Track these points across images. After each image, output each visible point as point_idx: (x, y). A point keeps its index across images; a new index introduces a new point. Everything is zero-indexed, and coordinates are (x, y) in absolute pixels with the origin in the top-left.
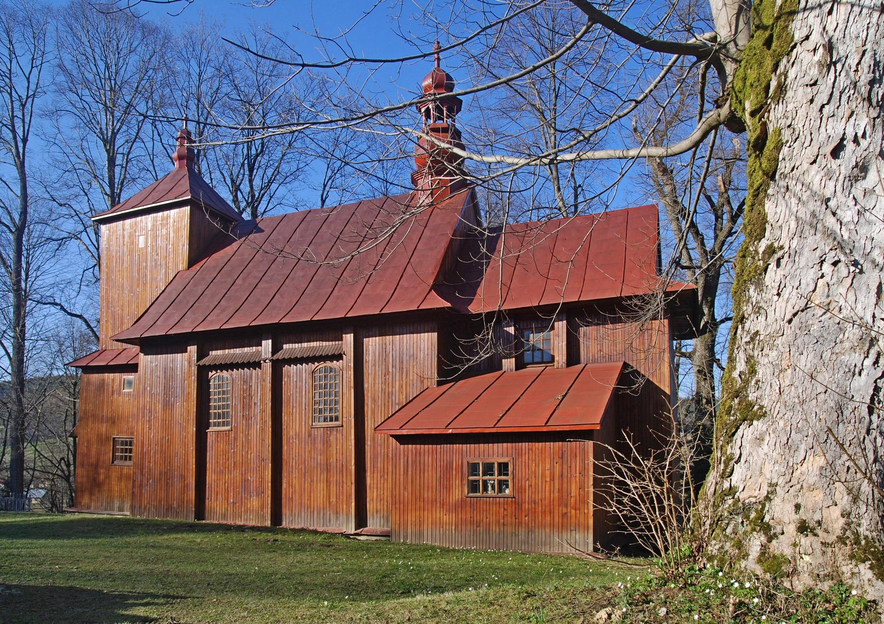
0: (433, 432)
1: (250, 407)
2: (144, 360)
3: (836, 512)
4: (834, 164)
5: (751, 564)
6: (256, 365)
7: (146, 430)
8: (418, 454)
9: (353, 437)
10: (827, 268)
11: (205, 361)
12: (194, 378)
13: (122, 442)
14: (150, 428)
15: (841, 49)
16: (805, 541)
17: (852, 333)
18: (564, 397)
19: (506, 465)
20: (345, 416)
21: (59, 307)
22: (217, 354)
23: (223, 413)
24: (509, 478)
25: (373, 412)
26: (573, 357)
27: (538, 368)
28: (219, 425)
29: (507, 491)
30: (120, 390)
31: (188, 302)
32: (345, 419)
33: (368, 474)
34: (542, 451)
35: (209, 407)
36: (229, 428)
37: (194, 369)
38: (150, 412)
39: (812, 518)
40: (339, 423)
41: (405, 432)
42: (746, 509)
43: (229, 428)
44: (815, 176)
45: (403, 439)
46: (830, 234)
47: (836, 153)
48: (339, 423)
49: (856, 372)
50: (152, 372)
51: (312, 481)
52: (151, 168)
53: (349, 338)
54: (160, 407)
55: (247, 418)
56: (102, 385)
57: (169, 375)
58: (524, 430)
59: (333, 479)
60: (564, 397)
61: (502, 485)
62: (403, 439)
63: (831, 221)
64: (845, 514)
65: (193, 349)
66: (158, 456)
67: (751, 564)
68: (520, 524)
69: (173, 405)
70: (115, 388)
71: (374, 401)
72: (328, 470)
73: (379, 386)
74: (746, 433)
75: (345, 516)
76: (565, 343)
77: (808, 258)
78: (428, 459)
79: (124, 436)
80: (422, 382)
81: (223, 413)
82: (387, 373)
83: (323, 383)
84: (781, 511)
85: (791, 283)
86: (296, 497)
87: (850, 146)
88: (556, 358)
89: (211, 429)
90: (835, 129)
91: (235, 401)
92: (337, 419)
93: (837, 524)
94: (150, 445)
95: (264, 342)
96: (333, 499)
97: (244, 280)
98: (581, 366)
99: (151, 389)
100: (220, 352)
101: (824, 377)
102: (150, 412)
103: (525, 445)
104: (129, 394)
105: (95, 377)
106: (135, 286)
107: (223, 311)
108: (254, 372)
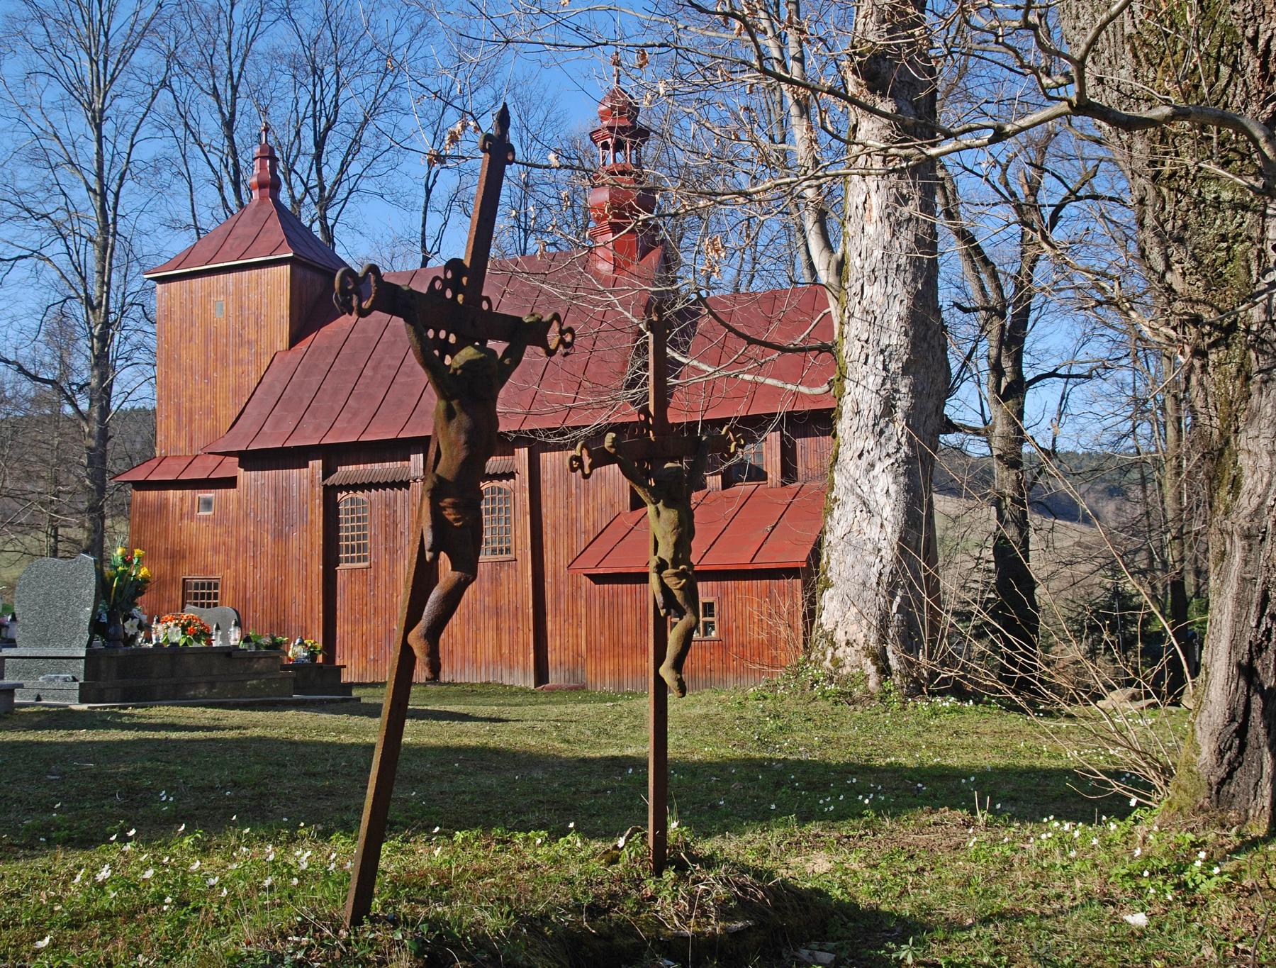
0: (633, 571)
1: (395, 537)
2: (242, 474)
3: (862, 635)
4: (859, 462)
5: (827, 664)
6: (405, 484)
7: (250, 569)
8: (615, 594)
9: (530, 573)
10: (858, 513)
11: (334, 479)
12: (319, 502)
13: (197, 584)
14: (255, 567)
15: (861, 406)
16: (848, 650)
17: (870, 546)
18: (774, 527)
19: (711, 605)
20: (519, 547)
21: (15, 367)
22: (347, 471)
23: (359, 545)
24: (715, 619)
25: (554, 543)
26: (789, 471)
27: (751, 486)
28: (353, 560)
29: (713, 634)
30: (193, 513)
31: (301, 401)
32: (518, 552)
33: (549, 618)
34: (749, 591)
35: (338, 539)
36: (367, 564)
37: (319, 491)
38: (255, 545)
39: (851, 638)
40: (509, 556)
41: (601, 571)
42: (827, 635)
43: (367, 564)
44: (851, 467)
45: (597, 579)
46: (859, 496)
47: (860, 456)
48: (509, 556)
49: (871, 566)
50: (256, 493)
51: (478, 629)
52: (185, 171)
53: (523, 453)
54: (268, 539)
55: (392, 552)
56: (163, 507)
57: (281, 496)
58: (729, 568)
59: (505, 626)
60: (774, 527)
61: (708, 626)
62: (597, 579)
63: (858, 490)
64: (865, 636)
65: (316, 465)
66: (267, 603)
67: (827, 664)
68: (728, 669)
69: (287, 536)
70: (185, 510)
71: (555, 528)
72: (498, 615)
73: (560, 512)
74: (827, 594)
75: (521, 670)
76: (779, 457)
77: (849, 507)
78: (627, 600)
79: (197, 577)
80: (613, 506)
81: (359, 545)
82: (569, 495)
83: (489, 506)
84: (840, 636)
85: (844, 519)
86: (458, 650)
87: (866, 454)
88: (769, 476)
89: (342, 566)
90: (860, 444)
91: (374, 531)
92: (508, 550)
93: (861, 640)
94: (255, 589)
95: (412, 457)
96: (505, 650)
97: (375, 369)
98: (798, 484)
99: (256, 515)
100: (352, 468)
101: (858, 568)
102: (255, 545)
103: (730, 584)
104: (206, 519)
105: (152, 495)
106: (211, 369)
107: (355, 415)
108: (400, 494)
